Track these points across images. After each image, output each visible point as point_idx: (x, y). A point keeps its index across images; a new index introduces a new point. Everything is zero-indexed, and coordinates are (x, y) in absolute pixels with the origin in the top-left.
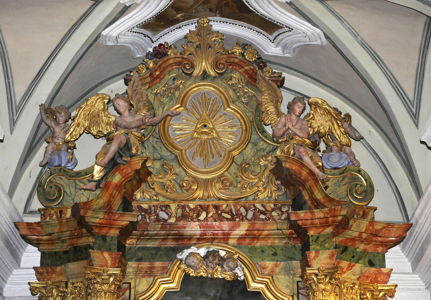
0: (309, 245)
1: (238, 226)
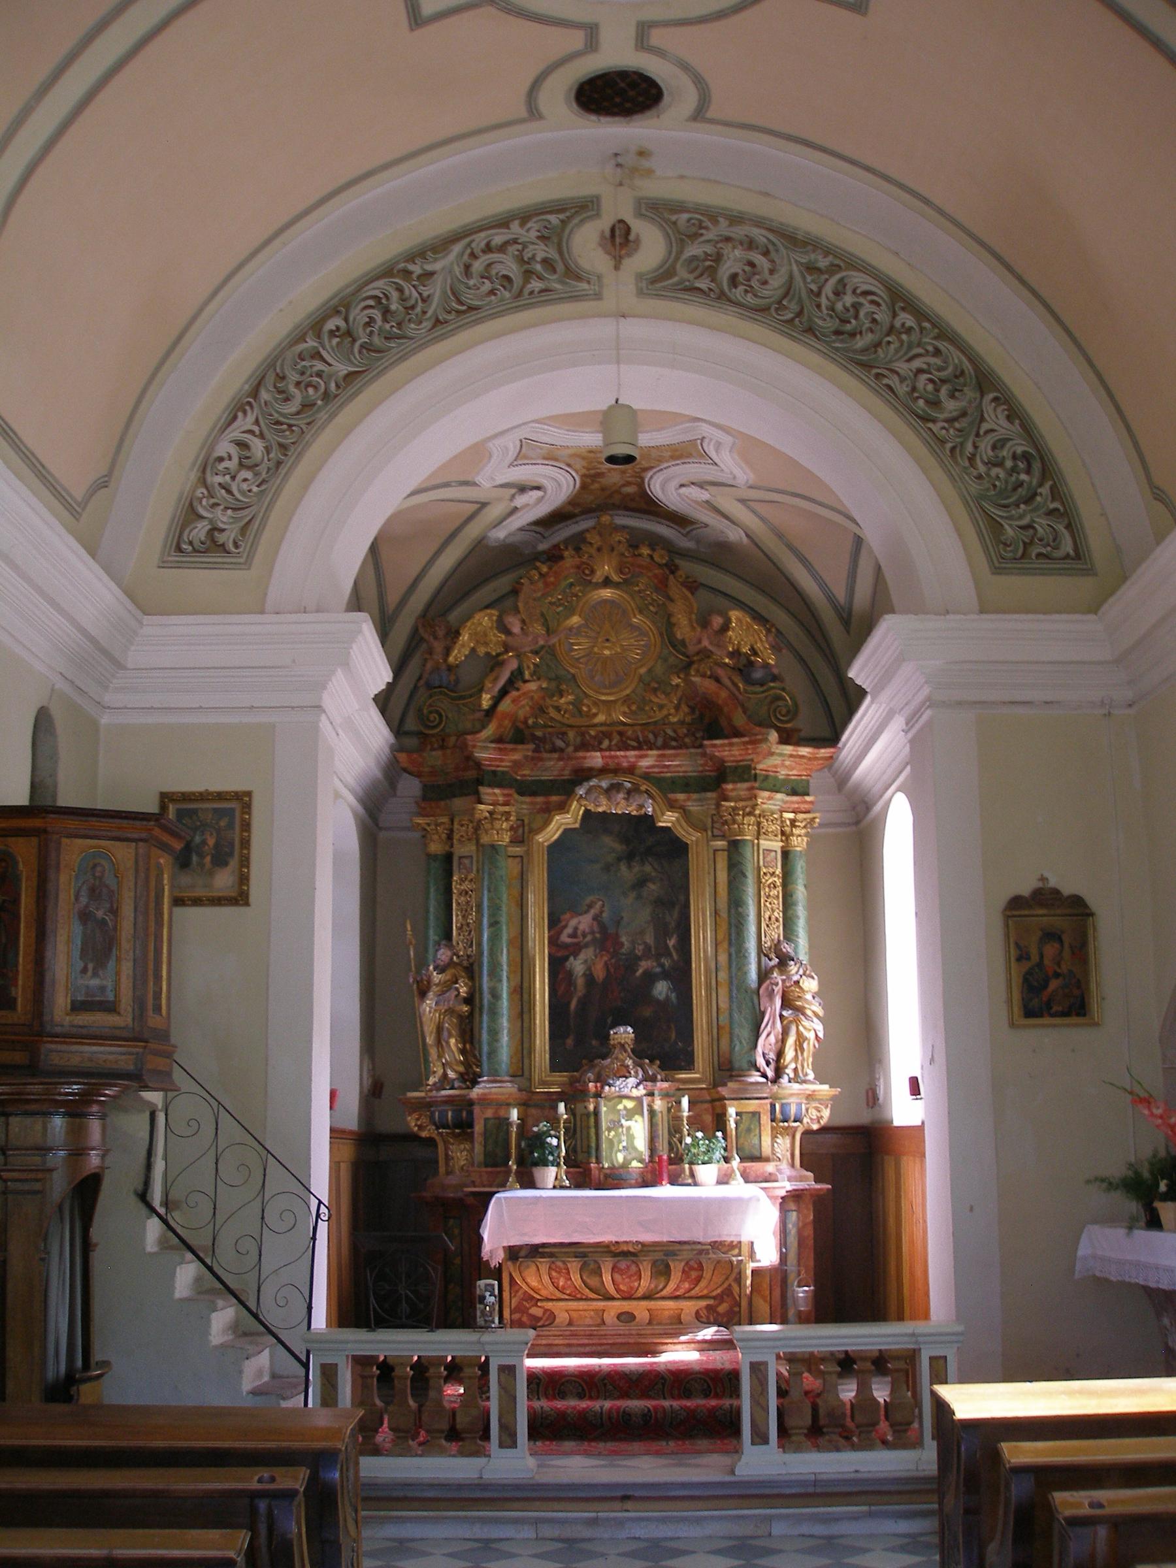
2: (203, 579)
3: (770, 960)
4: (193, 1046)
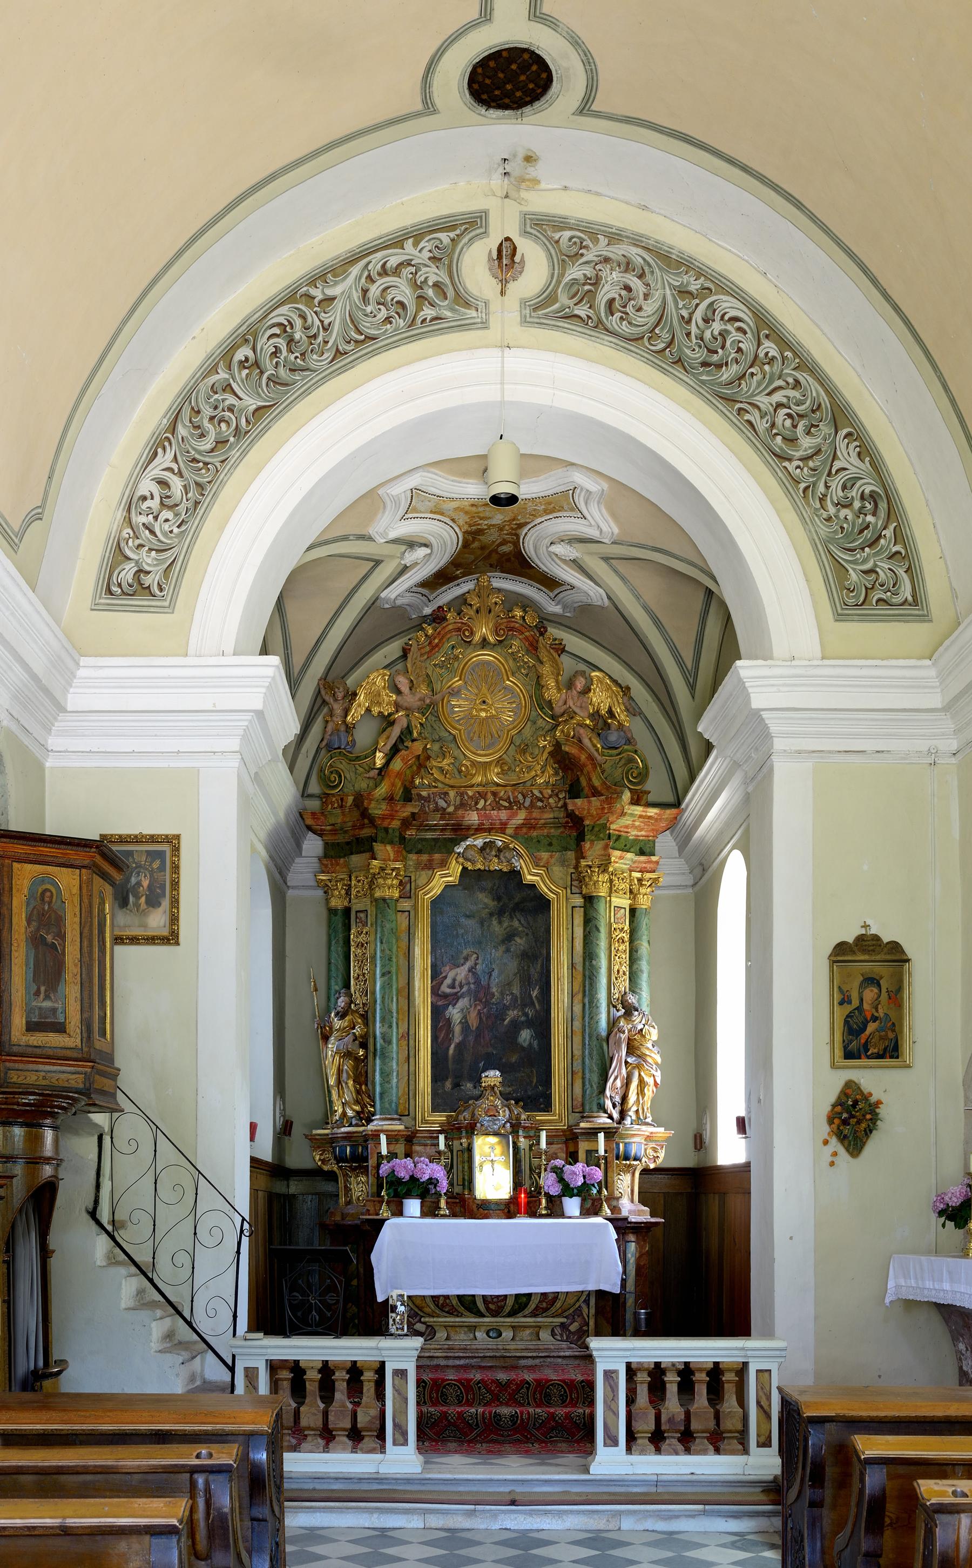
0: (584, 836)
1: (517, 814)
2: (130, 622)
3: (618, 1011)
4: (134, 1075)
